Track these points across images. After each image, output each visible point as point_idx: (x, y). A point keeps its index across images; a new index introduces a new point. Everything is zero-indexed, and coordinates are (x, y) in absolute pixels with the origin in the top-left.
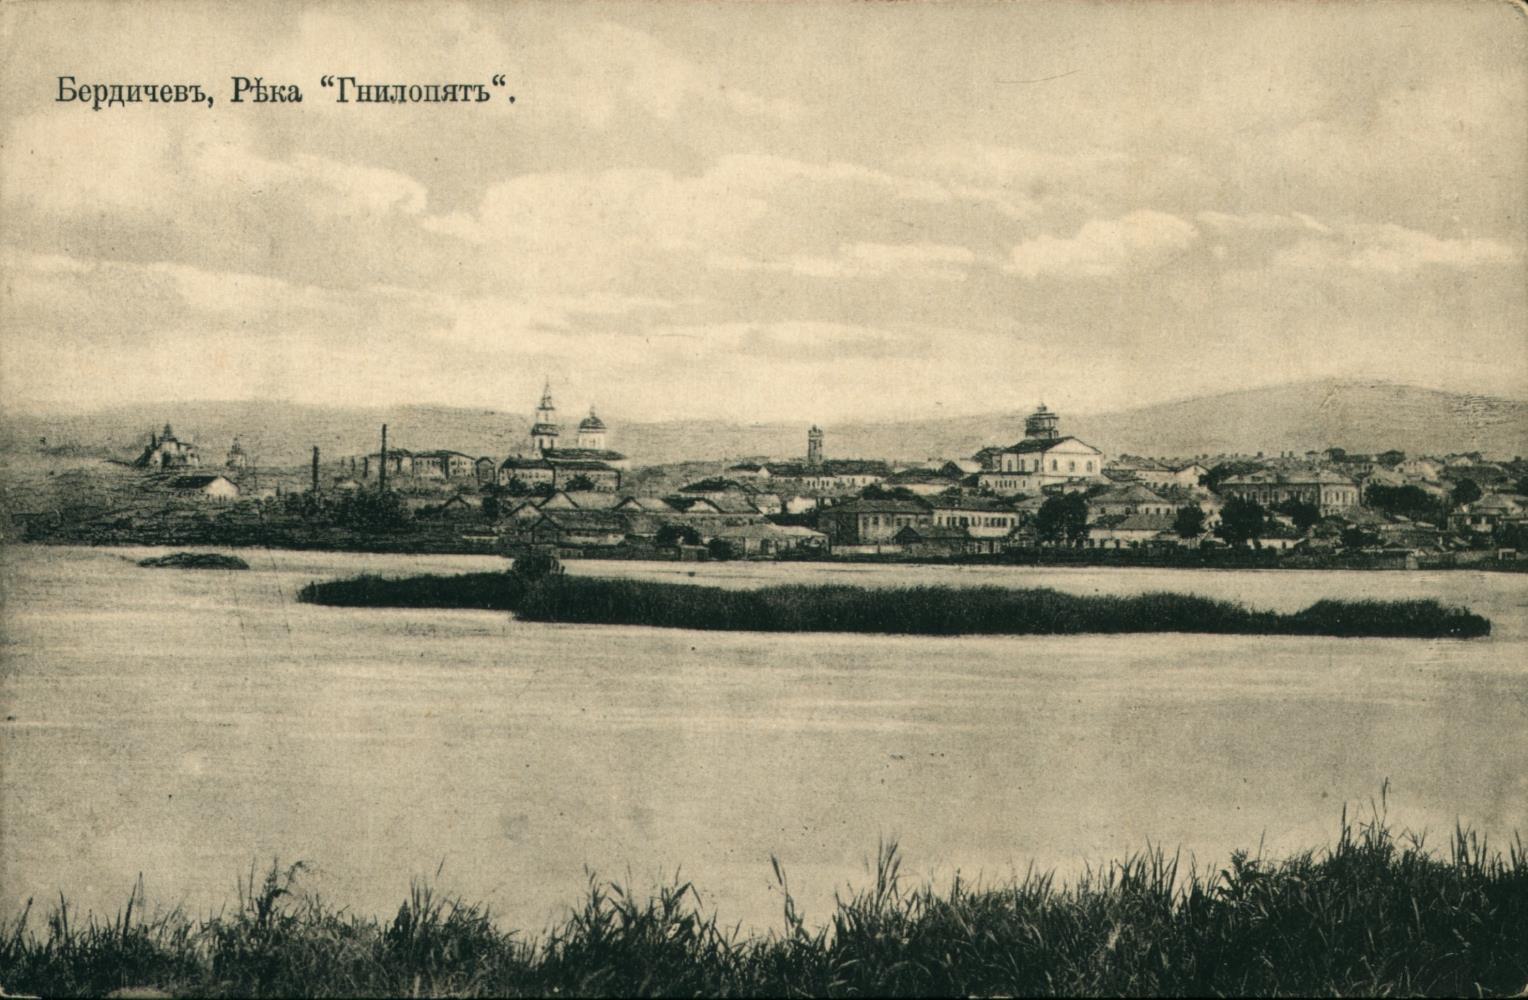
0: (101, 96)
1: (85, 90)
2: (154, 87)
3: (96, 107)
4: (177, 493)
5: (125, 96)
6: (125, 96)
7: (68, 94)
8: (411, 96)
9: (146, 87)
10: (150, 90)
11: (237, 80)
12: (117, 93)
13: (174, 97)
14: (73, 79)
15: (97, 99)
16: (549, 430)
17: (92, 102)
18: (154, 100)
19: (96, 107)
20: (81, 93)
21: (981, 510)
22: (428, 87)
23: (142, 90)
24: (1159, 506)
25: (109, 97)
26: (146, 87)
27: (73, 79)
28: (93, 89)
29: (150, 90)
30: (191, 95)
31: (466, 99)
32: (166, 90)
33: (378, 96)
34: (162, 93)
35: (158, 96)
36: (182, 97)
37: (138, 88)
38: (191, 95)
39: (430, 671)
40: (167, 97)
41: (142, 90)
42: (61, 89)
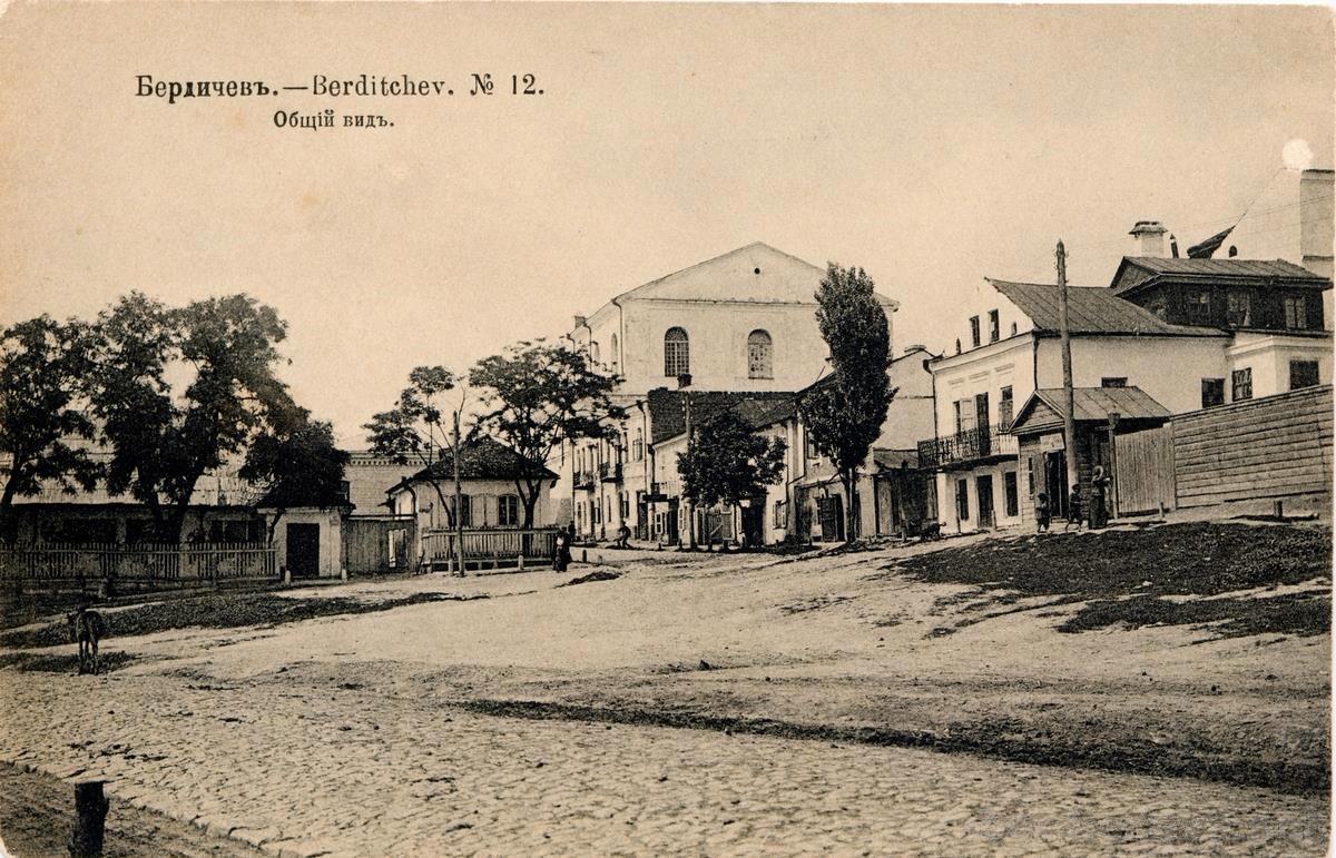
2: (221, 83)
3: (172, 101)
4: (1263, 815)
9: (214, 84)
10: (218, 86)
11: (346, 118)
14: (150, 77)
15: (172, 94)
17: (168, 95)
19: (172, 101)
20: (331, 87)
22: (413, 93)
26: (214, 84)
27: (150, 77)
28: (168, 87)
29: (218, 86)
31: (346, 93)
33: (207, 88)
34: (228, 88)
35: (225, 91)
37: (207, 84)
38: (255, 89)
40: (232, 92)
41: (211, 86)
42: (140, 85)
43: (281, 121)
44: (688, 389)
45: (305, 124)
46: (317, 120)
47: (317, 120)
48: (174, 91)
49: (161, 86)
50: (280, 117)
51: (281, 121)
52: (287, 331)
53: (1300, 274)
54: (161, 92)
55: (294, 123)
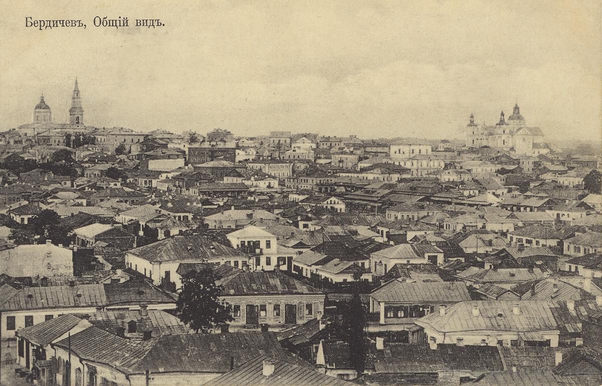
0: (42, 24)
1: (36, 22)
2: (63, 21)
5: (52, 25)
6: (52, 25)
7: (29, 24)
8: (103, 24)
9: (60, 21)
10: (61, 22)
11: (137, 20)
12: (152, 23)
13: (71, 25)
14: (31, 18)
16: (398, 142)
17: (39, 27)
18: (63, 26)
21: (343, 172)
22: (110, 21)
23: (58, 22)
24: (421, 147)
25: (45, 25)
28: (39, 22)
29: (61, 22)
30: (77, 24)
32: (68, 22)
35: (65, 25)
36: (74, 25)
38: (77, 24)
39: (460, 340)
40: (68, 25)
41: (58, 22)
43: (97, 23)
44: (576, 265)
45: (111, 25)
46: (118, 22)
47: (118, 22)
48: (42, 24)
49: (36, 22)
50: (97, 20)
51: (97, 23)
52: (228, 131)
53: (369, 172)
54: (36, 25)
55: (105, 24)
